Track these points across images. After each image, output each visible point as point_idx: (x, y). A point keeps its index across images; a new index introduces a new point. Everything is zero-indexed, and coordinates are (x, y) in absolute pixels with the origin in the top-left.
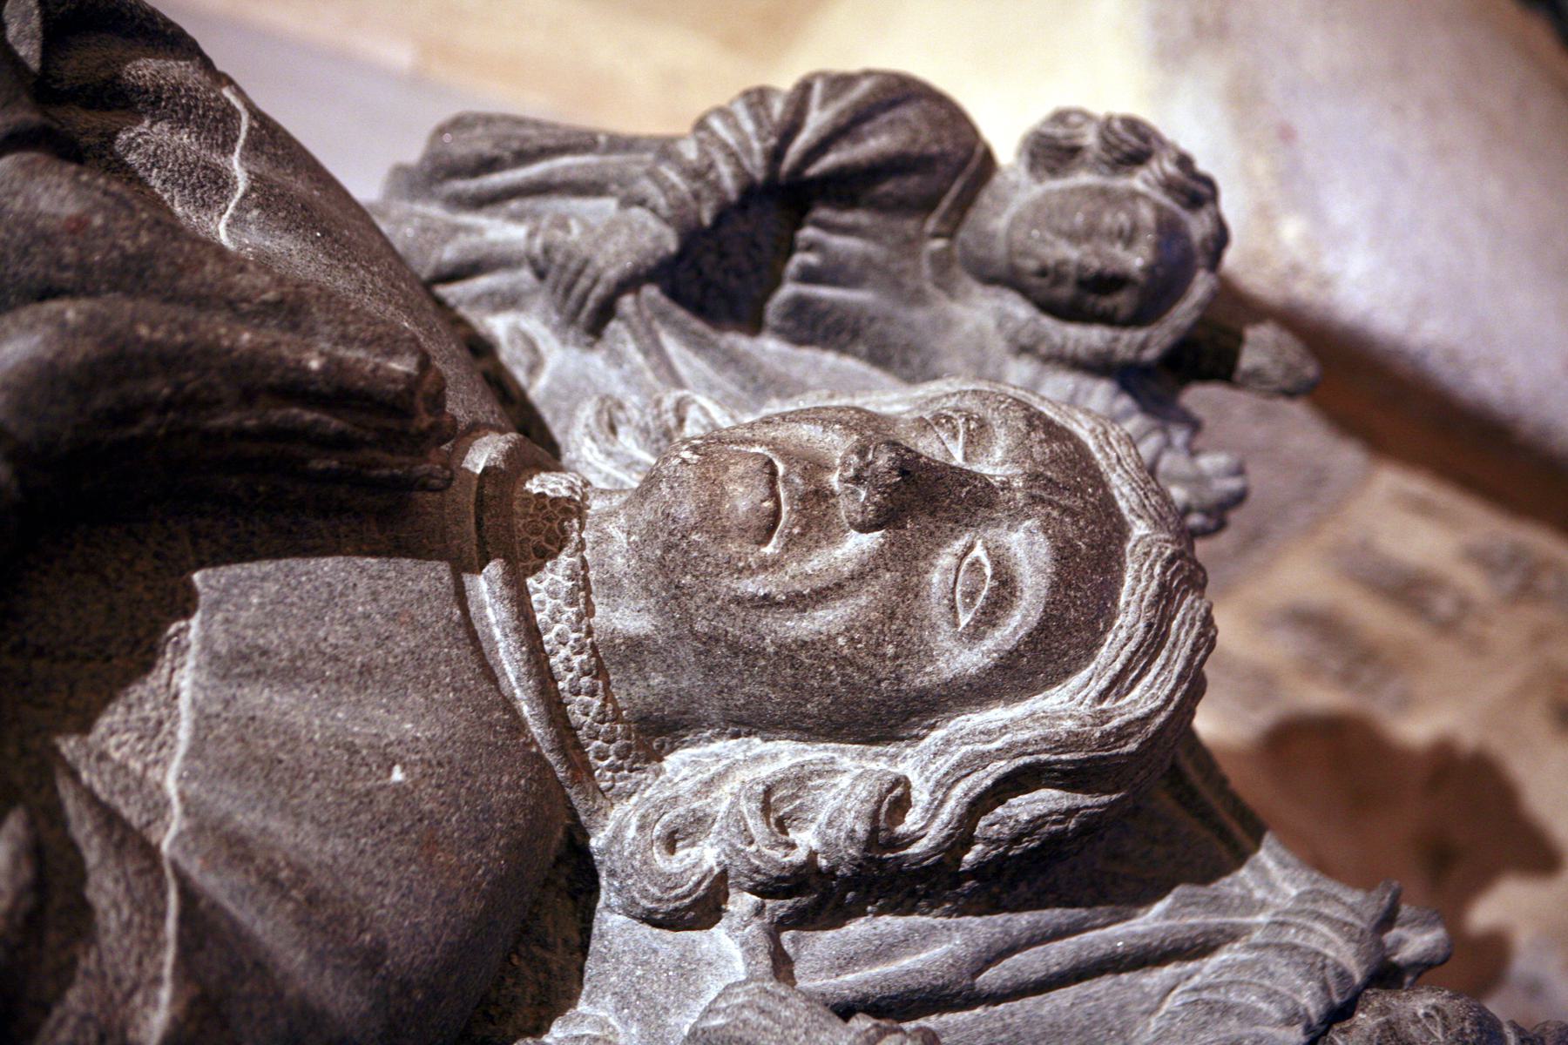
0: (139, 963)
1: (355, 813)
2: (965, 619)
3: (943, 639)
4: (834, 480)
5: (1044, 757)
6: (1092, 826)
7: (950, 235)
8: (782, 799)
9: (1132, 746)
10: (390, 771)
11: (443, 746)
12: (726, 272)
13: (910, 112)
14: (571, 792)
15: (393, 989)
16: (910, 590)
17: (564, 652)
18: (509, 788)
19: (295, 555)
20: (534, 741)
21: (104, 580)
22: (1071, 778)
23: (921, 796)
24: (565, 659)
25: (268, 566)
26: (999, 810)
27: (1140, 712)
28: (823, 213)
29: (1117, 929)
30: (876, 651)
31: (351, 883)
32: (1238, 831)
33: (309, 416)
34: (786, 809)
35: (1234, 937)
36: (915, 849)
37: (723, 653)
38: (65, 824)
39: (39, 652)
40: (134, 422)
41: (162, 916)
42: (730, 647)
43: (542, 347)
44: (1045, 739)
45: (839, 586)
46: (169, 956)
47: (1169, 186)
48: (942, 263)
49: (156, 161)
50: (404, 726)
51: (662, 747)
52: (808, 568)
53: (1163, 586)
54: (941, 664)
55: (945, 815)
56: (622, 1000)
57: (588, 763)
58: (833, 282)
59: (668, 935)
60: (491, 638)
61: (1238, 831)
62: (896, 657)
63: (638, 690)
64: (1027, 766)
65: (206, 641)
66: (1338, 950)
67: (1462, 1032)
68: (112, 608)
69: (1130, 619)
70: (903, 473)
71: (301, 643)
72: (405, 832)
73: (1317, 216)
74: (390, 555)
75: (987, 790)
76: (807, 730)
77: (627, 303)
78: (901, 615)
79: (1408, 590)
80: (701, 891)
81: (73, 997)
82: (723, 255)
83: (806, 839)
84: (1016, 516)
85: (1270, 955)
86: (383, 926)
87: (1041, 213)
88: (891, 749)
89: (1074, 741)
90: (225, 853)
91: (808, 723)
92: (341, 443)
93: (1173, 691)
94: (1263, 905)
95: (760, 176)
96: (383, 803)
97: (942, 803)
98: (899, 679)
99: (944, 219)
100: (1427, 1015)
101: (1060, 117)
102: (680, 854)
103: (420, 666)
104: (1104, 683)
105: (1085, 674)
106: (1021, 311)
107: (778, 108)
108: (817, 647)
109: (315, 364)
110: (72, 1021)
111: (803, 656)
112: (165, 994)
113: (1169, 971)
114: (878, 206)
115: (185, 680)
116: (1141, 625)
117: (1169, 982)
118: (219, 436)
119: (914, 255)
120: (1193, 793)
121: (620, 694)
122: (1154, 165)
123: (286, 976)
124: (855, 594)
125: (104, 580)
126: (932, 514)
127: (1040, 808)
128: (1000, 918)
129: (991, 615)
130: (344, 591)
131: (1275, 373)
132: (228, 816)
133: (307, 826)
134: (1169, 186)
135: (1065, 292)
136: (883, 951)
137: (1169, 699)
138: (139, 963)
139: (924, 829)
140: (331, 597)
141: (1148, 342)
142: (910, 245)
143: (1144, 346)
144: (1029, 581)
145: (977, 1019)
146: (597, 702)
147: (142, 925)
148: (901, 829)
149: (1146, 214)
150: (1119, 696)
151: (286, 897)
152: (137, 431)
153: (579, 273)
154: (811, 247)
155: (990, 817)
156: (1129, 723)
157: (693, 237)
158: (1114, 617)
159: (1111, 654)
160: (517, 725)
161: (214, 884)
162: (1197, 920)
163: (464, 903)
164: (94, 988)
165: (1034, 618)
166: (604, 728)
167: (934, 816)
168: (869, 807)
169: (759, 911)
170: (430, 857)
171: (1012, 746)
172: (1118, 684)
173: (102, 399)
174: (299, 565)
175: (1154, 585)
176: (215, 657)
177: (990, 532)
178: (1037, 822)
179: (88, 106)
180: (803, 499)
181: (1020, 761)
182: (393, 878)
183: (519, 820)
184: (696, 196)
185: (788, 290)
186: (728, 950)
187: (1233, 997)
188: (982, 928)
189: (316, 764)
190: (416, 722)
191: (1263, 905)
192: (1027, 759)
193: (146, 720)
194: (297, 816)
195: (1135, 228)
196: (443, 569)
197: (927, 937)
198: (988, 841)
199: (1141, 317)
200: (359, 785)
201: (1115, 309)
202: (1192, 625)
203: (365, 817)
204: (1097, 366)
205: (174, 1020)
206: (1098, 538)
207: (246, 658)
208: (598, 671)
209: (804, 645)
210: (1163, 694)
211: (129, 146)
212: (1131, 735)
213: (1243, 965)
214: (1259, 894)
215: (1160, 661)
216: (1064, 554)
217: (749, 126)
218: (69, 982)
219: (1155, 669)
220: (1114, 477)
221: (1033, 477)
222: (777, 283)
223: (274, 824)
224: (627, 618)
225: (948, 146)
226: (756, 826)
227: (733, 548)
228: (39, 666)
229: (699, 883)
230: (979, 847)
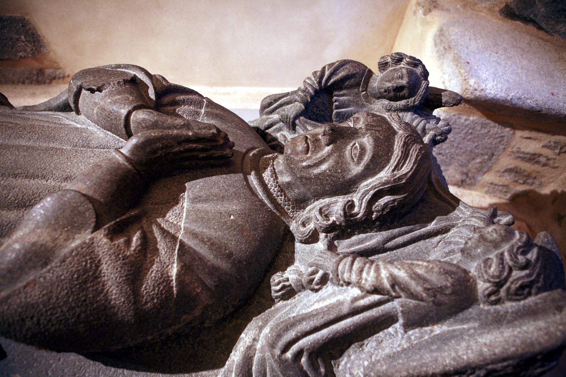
0: (169, 259)
1: (223, 226)
2: (355, 160)
3: (352, 166)
4: (320, 137)
5: (381, 188)
6: (402, 204)
7: (366, 90)
8: (325, 210)
9: (404, 181)
10: (230, 217)
11: (243, 210)
12: (320, 111)
13: (348, 66)
14: (282, 218)
15: (236, 262)
16: (341, 157)
17: (273, 188)
18: (262, 218)
19: (207, 177)
20: (269, 208)
21: (168, 188)
22: (392, 191)
23: (357, 203)
24: (273, 190)
25: (201, 180)
26: (377, 203)
27: (404, 173)
28: (336, 93)
29: (423, 229)
30: (336, 171)
31: (223, 241)
32: (453, 202)
33: (194, 146)
34: (327, 212)
35: (453, 226)
36: (359, 216)
37: (306, 180)
38: (154, 234)
39: (156, 204)
40: (157, 153)
41: (175, 250)
42: (305, 178)
43: (287, 136)
44: (380, 183)
45: (324, 159)
46: (176, 258)
47: (408, 64)
48: (366, 97)
49: (184, 112)
50: (234, 207)
51: (304, 206)
52: (317, 157)
53: (405, 143)
54: (353, 172)
55: (363, 207)
56: (300, 262)
57: (285, 212)
58: (343, 108)
59: (308, 245)
60: (255, 188)
61: (453, 202)
62: (341, 172)
63: (293, 194)
64: (377, 191)
65: (188, 196)
66: (479, 224)
67: (501, 233)
68: (169, 193)
69: (397, 151)
70: (332, 130)
71: (208, 193)
72: (235, 229)
73: (478, 77)
74: (228, 174)
75: (371, 198)
76: (329, 194)
77: (297, 122)
78: (340, 163)
79: (533, 158)
80: (310, 234)
81: (154, 267)
82: (318, 108)
83: (333, 219)
84: (364, 135)
85: (461, 228)
86: (232, 249)
87: (382, 80)
88: (351, 195)
89: (387, 182)
90: (191, 237)
91: (328, 192)
92: (203, 150)
93: (413, 167)
94: (461, 218)
95: (318, 88)
96: (229, 223)
97: (361, 204)
98: (344, 177)
99: (363, 87)
100: (492, 231)
101: (382, 58)
102: (307, 227)
103: (236, 194)
104: (393, 168)
105: (388, 167)
106: (386, 102)
107: (318, 74)
108: (323, 173)
109: (190, 134)
110: (154, 272)
111: (320, 177)
112: (175, 265)
113: (439, 237)
114: (346, 88)
115: (185, 205)
116: (400, 152)
117: (439, 240)
118: (175, 153)
119: (359, 97)
120: (440, 195)
121: (289, 195)
122: (404, 60)
123: (208, 261)
124: (328, 160)
125: (168, 188)
126: (343, 138)
127: (386, 201)
128: (390, 231)
129: (361, 157)
130: (218, 182)
131: (451, 100)
132: (194, 230)
133: (212, 230)
134: (408, 64)
135: (392, 94)
136: (361, 242)
137: (412, 169)
138: (169, 259)
139: (359, 210)
140: (215, 183)
141: (416, 100)
142: (358, 94)
143: (414, 101)
144: (369, 148)
145: (388, 255)
146: (283, 198)
147: (169, 252)
148: (353, 212)
149: (404, 71)
150: (398, 170)
151: (206, 244)
152: (158, 155)
153: (287, 118)
154: (336, 101)
155: (375, 206)
156: (401, 176)
157: (307, 105)
158: (393, 152)
159: (393, 161)
160: (263, 204)
161: (190, 243)
162: (443, 224)
163: (253, 243)
164: (159, 265)
165: (371, 155)
166: (287, 203)
167: (361, 208)
168: (342, 208)
169: (326, 237)
170: (242, 234)
171: (372, 187)
172: (397, 167)
173: (148, 150)
174: (207, 179)
175: (402, 143)
176: (191, 199)
177: (359, 140)
178: (386, 204)
179: (171, 106)
180: (313, 142)
181: (376, 190)
182: (234, 239)
183: (266, 224)
184: (305, 96)
185: (335, 111)
186: (321, 245)
187: (452, 240)
188: (385, 234)
189: (212, 217)
190: (236, 206)
191: (461, 218)
192: (377, 189)
193: (176, 213)
194: (210, 228)
195: (402, 75)
196: (241, 175)
197: (371, 238)
198: (377, 211)
199: (410, 95)
200: (223, 220)
201: (405, 94)
202: (416, 151)
203: (225, 227)
204: (406, 109)
205: (178, 270)
206: (386, 135)
207: (196, 198)
208: (281, 190)
209: (320, 174)
210: (410, 168)
211: (179, 111)
212: (402, 179)
213: (456, 232)
214: (460, 216)
215: (408, 160)
216: (376, 141)
217: (313, 79)
218: (153, 264)
219: (407, 162)
220: (393, 123)
221: (367, 125)
222: (332, 111)
223: (204, 230)
224: (285, 178)
225: (358, 71)
226: (319, 217)
227: (300, 156)
228: (156, 206)
229: (309, 232)
230: (375, 213)
